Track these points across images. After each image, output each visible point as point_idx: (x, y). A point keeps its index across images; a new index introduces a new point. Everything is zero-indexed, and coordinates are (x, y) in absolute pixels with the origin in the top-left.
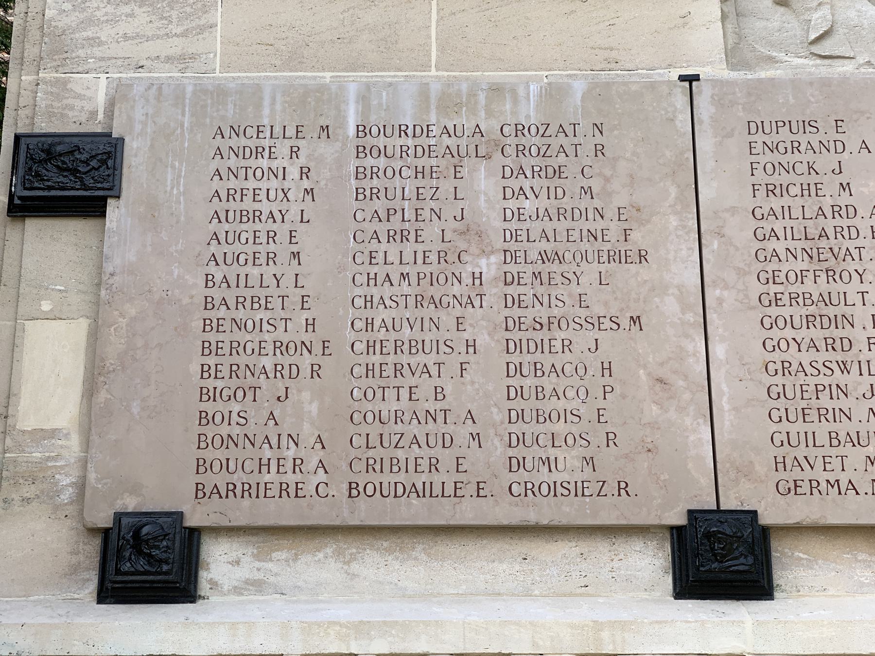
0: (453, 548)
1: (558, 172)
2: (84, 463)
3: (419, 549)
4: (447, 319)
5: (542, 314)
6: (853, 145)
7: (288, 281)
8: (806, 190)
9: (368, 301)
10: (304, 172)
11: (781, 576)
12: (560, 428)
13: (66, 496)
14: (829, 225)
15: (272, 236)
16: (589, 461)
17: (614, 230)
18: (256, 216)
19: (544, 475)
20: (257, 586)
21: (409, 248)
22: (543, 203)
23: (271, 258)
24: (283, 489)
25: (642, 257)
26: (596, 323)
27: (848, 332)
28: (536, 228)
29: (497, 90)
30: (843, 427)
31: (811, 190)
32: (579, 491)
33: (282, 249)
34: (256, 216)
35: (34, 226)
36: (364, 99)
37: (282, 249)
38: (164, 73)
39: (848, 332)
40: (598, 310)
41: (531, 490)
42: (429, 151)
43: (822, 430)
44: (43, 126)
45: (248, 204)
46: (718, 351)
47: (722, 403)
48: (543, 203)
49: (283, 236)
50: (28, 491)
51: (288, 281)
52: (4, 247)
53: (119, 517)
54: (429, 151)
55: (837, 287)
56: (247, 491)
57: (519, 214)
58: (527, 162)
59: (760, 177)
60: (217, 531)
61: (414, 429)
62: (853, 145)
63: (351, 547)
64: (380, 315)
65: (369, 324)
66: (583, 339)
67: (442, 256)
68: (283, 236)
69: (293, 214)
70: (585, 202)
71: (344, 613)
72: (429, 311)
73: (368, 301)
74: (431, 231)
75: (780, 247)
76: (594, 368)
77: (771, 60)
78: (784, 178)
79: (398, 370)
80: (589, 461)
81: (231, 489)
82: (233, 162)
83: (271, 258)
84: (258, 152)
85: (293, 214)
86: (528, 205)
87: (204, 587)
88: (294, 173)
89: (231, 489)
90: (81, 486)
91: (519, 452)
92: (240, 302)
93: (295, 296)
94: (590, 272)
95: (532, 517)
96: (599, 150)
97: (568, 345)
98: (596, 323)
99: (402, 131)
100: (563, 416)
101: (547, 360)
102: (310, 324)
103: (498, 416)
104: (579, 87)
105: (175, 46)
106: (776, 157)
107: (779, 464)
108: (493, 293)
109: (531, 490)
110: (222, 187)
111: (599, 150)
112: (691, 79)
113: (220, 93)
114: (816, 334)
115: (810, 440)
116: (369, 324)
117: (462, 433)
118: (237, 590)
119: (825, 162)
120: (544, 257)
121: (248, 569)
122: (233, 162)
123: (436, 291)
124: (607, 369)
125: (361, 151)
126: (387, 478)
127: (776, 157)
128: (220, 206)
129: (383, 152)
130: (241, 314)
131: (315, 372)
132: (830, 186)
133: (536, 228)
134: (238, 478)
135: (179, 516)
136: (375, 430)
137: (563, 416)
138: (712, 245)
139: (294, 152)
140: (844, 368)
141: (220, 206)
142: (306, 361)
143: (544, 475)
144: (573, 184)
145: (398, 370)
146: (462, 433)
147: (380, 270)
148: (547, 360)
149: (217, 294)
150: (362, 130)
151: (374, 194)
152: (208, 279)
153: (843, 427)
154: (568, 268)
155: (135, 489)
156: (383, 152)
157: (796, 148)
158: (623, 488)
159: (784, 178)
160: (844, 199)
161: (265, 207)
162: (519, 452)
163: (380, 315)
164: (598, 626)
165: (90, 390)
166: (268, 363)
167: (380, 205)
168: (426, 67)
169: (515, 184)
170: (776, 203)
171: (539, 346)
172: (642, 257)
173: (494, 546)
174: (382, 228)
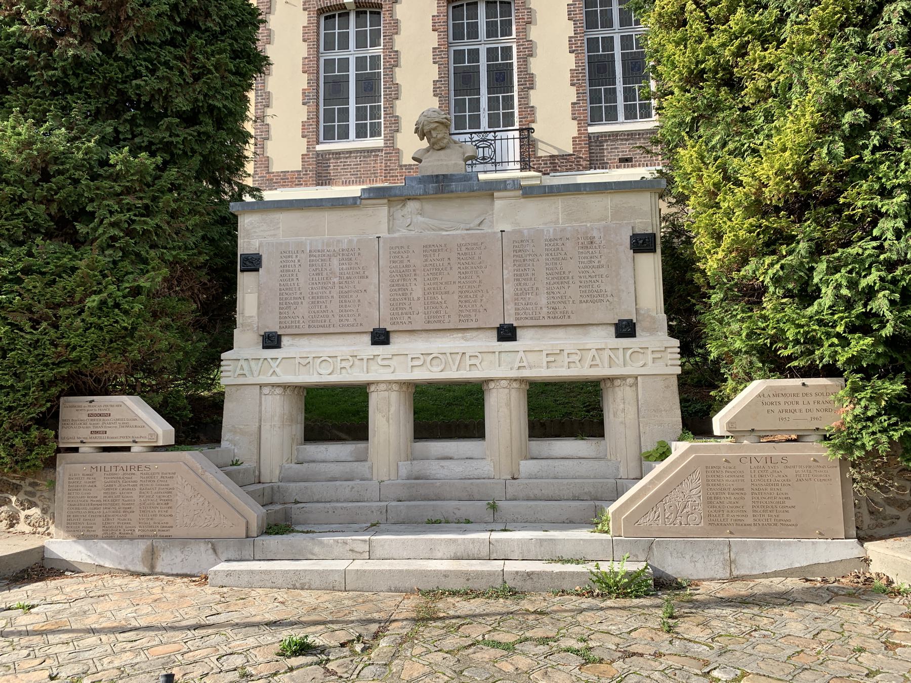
0: (328, 337)
1: (351, 259)
2: (258, 322)
3: (323, 337)
4: (328, 292)
5: (346, 290)
6: (411, 252)
7: (296, 284)
8: (401, 262)
9: (312, 288)
10: (299, 261)
11: (391, 340)
12: (350, 313)
13: (256, 329)
14: (404, 269)
15: (292, 275)
16: (355, 319)
17: (362, 272)
18: (289, 271)
19: (346, 322)
20: (292, 345)
21: (320, 277)
22: (347, 266)
23: (292, 280)
24: (296, 327)
25: (367, 277)
26: (357, 291)
27: (407, 292)
28: (346, 271)
29: (338, 241)
30: (404, 311)
31: (401, 262)
32: (353, 325)
33: (295, 278)
34: (289, 271)
35: (245, 273)
36: (311, 244)
37: (295, 278)
38: (270, 239)
39: (407, 292)
40: (358, 288)
41: (344, 325)
42: (324, 255)
43: (400, 312)
44: (246, 252)
45: (288, 268)
46: (381, 296)
47: (381, 307)
48: (347, 266)
49: (295, 275)
50: (248, 328)
51: (296, 284)
52: (206, 539)
53: (265, 333)
54: (324, 255)
55: (405, 283)
56: (289, 327)
57: (342, 269)
58: (344, 257)
59: (392, 259)
60: (284, 335)
61: (321, 314)
62: (411, 252)
63: (310, 337)
64: (314, 291)
65: (312, 293)
66: (355, 295)
67: (327, 278)
68: (295, 275)
69: (297, 270)
70: (356, 266)
71: (307, 350)
72: (324, 290)
73: (312, 288)
74: (325, 273)
75: (394, 274)
76: (357, 301)
77: (399, 230)
78: (396, 259)
79: (318, 302)
80: (355, 319)
81: (286, 327)
82: (284, 259)
83: (292, 280)
84: (289, 257)
85: (297, 270)
86: (344, 267)
87: (282, 346)
88: (297, 261)
89: (286, 327)
90: (258, 327)
91: (342, 318)
92: (287, 289)
93: (298, 287)
94: (356, 281)
95: (343, 331)
96: (359, 254)
97: (351, 296)
98: (357, 291)
99: (319, 251)
100: (350, 311)
101: (347, 299)
102: (301, 293)
103: (338, 311)
104: (355, 239)
105: (272, 232)
106: (395, 255)
107: (391, 319)
108: (337, 286)
109: (344, 325)
110: (282, 265)
111: (359, 254)
112: (378, 237)
113: (281, 244)
114: (401, 292)
115: (398, 314)
116: (312, 293)
117: (331, 315)
118: (288, 346)
119: (405, 255)
120: (347, 278)
121: (291, 342)
122: (284, 259)
123: (326, 286)
124: (359, 301)
125: (310, 256)
126: (316, 324)
127: (395, 255)
128: (282, 269)
129: (315, 256)
130: (287, 292)
131: (302, 303)
132: (406, 260)
133: (346, 271)
134: (288, 325)
135: (230, 347)
136: (313, 314)
137: (350, 311)
138: (381, 274)
139: (296, 256)
140: (405, 299)
141: (282, 269)
142: (300, 301)
143: (346, 322)
144: (353, 262)
145: (318, 302)
146: (331, 315)
147: (314, 282)
148: (347, 299)
149: (282, 287)
150: (310, 251)
151: (313, 265)
152: (280, 285)
153: (404, 311)
154: (352, 280)
155: (268, 328)
156: (315, 256)
157: (399, 253)
158: (361, 325)
159: (396, 259)
160: (408, 263)
161: (291, 269)
162: (342, 318)
163: (314, 291)
164: (354, 351)
165: (258, 308)
166: (292, 301)
167: (314, 268)
168: (324, 235)
169: (341, 262)
170: (394, 265)
171: (346, 297)
172: (367, 277)
173: (337, 336)
174: (315, 273)
